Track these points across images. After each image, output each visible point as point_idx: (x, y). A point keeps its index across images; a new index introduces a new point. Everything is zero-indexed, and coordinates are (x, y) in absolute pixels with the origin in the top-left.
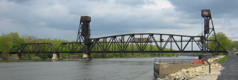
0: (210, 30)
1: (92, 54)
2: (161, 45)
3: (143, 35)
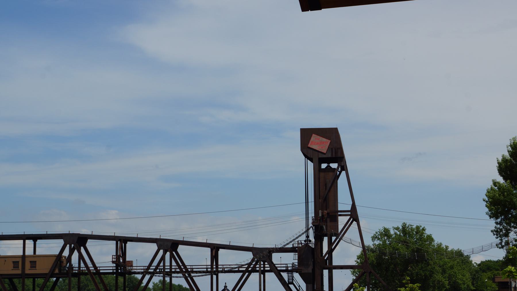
0: (342, 221)
3: (39, 242)
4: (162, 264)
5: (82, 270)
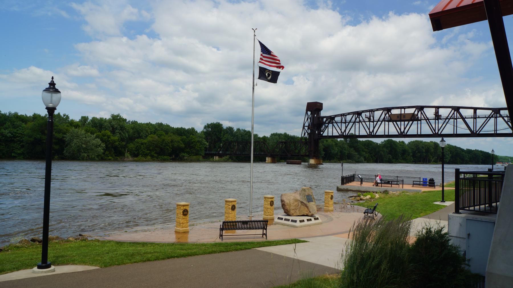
2: (475, 124)
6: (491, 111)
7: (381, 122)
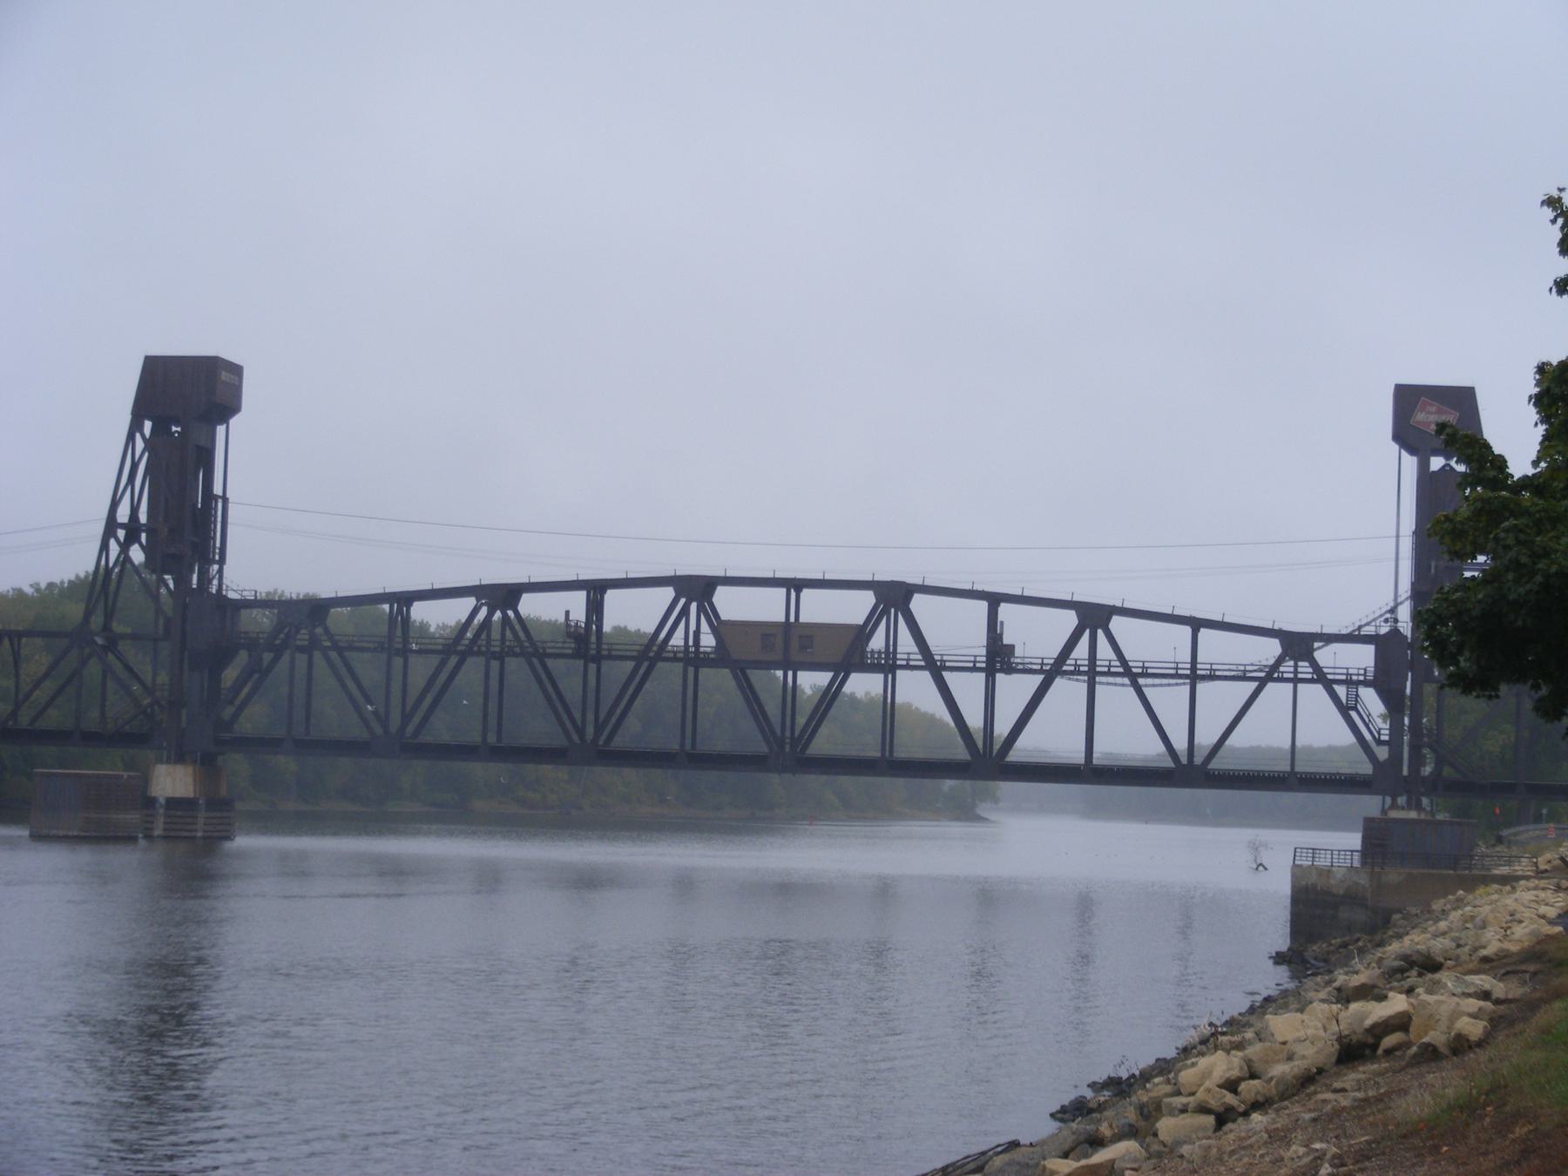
1: (237, 765)
4: (484, 636)
5: (705, 653)
6: (470, 602)
7: (1254, 685)
